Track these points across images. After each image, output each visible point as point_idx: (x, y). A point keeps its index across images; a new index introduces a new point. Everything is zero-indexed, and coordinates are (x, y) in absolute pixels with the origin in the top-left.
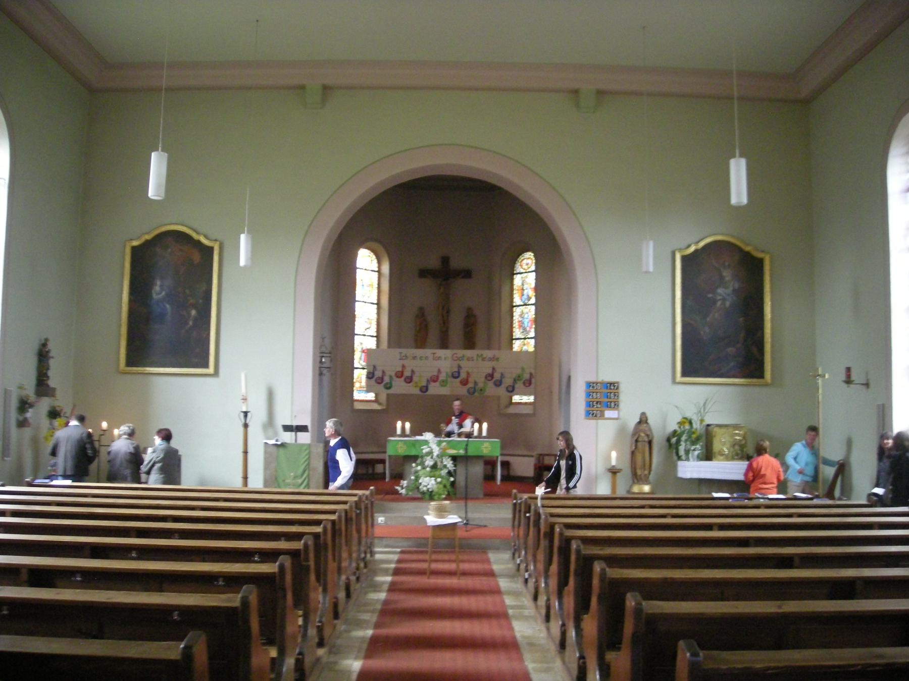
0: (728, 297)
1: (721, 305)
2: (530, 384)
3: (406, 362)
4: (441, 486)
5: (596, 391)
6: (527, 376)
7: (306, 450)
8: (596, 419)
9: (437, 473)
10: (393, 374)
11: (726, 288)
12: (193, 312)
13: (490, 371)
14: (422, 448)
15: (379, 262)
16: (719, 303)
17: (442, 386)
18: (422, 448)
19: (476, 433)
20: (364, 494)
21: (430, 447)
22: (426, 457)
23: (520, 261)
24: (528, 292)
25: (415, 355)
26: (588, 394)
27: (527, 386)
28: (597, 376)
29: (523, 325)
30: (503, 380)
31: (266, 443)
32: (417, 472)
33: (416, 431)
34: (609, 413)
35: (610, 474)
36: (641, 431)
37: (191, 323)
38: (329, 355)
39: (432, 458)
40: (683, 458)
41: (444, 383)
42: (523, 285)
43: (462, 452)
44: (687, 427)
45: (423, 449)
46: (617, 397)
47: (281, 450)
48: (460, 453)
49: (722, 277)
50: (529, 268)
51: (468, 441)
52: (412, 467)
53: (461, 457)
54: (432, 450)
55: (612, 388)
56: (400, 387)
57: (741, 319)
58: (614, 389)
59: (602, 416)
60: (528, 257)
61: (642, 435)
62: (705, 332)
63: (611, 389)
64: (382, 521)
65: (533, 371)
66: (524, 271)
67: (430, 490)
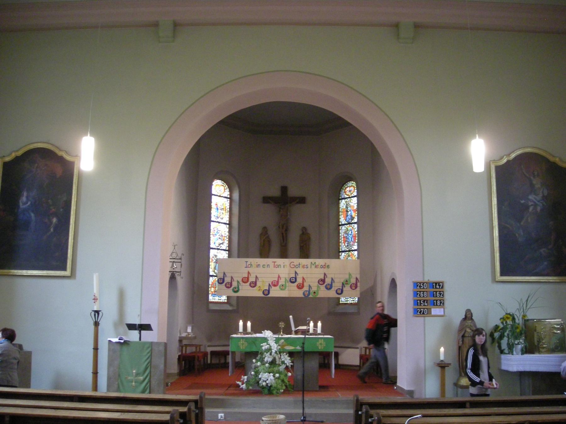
0: (538, 203)
1: (532, 210)
2: (356, 287)
3: (251, 270)
4: (280, 381)
5: (423, 290)
6: (353, 281)
7: (148, 348)
8: (424, 317)
9: (276, 369)
10: (240, 280)
11: (537, 195)
12: (55, 220)
13: (322, 277)
14: (261, 345)
15: (231, 191)
16: (531, 209)
17: (281, 289)
18: (261, 345)
19: (311, 331)
20: (202, 392)
21: (269, 344)
22: (265, 353)
23: (344, 189)
24: (351, 214)
25: (258, 264)
26: (416, 294)
27: (354, 289)
28: (424, 278)
29: (348, 240)
30: (333, 284)
31: (110, 341)
32: (256, 367)
33: (256, 329)
34: (435, 311)
35: (439, 369)
36: (467, 327)
37: (52, 230)
38: (179, 261)
39: (271, 354)
40: (506, 351)
41: (283, 288)
42: (347, 207)
43: (299, 348)
44: (510, 322)
45: (262, 346)
46: (443, 295)
47: (125, 348)
48: (297, 349)
49: (532, 185)
50: (351, 194)
51: (305, 337)
52: (253, 363)
53: (299, 353)
54: (270, 346)
55: (438, 287)
56: (246, 291)
57: (551, 223)
58: (439, 288)
59: (429, 312)
60: (350, 185)
61: (468, 330)
62: (520, 236)
63: (437, 288)
64: (222, 417)
65: (358, 277)
66: (348, 197)
67: (269, 385)
